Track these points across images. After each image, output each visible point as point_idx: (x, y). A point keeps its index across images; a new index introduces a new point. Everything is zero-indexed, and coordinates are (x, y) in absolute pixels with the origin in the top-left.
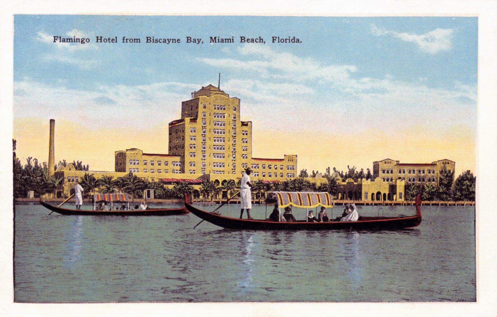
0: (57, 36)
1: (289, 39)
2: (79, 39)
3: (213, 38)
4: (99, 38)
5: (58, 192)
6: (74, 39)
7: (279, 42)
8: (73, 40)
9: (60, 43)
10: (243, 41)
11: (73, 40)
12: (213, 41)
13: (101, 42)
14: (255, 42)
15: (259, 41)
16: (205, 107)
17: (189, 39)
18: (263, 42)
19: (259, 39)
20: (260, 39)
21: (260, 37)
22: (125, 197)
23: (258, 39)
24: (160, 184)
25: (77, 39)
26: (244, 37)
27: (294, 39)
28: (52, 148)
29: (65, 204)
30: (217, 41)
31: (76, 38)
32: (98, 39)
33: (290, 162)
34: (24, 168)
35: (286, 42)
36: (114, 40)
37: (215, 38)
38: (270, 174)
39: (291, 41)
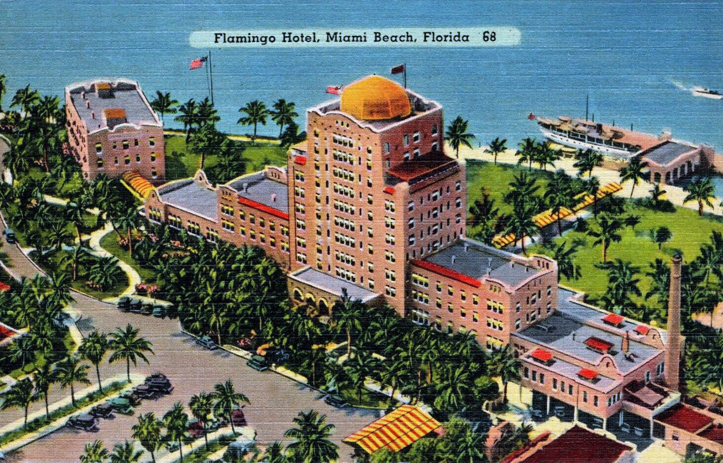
1: (451, 36)
3: (332, 35)
4: (287, 35)
5: (78, 168)
6: (249, 37)
7: (433, 41)
8: (247, 39)
11: (247, 39)
12: (332, 39)
15: (405, 39)
19: (406, 35)
20: (408, 36)
21: (407, 33)
22: (134, 190)
26: (380, 34)
27: (459, 36)
28: (262, 208)
30: (338, 39)
31: (251, 36)
32: (285, 37)
35: (445, 40)
38: (125, 143)
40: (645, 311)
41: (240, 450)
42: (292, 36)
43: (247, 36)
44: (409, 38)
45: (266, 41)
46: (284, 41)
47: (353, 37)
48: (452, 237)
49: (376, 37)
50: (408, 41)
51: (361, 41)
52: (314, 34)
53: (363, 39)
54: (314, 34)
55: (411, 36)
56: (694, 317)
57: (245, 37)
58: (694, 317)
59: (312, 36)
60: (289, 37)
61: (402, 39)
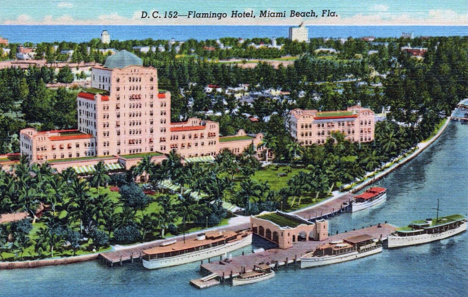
0: (326, 9)
2: (216, 14)
9: (194, 18)
10: (293, 15)
13: (236, 17)
14: (306, 16)
16: (118, 80)
17: (292, 12)
18: (314, 16)
19: (311, 12)
20: (312, 13)
23: (309, 13)
24: (141, 206)
25: (213, 14)
26: (294, 11)
29: (214, 280)
32: (233, 14)
33: (211, 145)
34: (70, 198)
36: (249, 14)
37: (266, 11)
39: (237, 15)
40: (103, 224)
41: (72, 174)
42: (238, 13)
43: (209, 13)
44: (313, 14)
45: (221, 17)
46: (232, 17)
47: (203, 14)
48: (132, 152)
49: (292, 13)
50: (311, 16)
51: (208, 17)
52: (252, 11)
53: (283, 15)
54: (252, 11)
55: (314, 13)
56: (49, 206)
57: (207, 14)
58: (49, 206)
59: (251, 13)
60: (236, 14)
61: (308, 15)
